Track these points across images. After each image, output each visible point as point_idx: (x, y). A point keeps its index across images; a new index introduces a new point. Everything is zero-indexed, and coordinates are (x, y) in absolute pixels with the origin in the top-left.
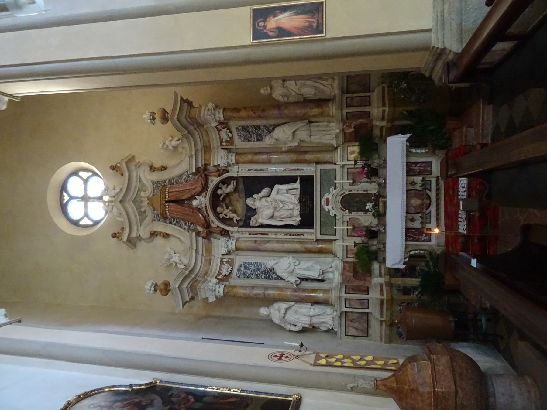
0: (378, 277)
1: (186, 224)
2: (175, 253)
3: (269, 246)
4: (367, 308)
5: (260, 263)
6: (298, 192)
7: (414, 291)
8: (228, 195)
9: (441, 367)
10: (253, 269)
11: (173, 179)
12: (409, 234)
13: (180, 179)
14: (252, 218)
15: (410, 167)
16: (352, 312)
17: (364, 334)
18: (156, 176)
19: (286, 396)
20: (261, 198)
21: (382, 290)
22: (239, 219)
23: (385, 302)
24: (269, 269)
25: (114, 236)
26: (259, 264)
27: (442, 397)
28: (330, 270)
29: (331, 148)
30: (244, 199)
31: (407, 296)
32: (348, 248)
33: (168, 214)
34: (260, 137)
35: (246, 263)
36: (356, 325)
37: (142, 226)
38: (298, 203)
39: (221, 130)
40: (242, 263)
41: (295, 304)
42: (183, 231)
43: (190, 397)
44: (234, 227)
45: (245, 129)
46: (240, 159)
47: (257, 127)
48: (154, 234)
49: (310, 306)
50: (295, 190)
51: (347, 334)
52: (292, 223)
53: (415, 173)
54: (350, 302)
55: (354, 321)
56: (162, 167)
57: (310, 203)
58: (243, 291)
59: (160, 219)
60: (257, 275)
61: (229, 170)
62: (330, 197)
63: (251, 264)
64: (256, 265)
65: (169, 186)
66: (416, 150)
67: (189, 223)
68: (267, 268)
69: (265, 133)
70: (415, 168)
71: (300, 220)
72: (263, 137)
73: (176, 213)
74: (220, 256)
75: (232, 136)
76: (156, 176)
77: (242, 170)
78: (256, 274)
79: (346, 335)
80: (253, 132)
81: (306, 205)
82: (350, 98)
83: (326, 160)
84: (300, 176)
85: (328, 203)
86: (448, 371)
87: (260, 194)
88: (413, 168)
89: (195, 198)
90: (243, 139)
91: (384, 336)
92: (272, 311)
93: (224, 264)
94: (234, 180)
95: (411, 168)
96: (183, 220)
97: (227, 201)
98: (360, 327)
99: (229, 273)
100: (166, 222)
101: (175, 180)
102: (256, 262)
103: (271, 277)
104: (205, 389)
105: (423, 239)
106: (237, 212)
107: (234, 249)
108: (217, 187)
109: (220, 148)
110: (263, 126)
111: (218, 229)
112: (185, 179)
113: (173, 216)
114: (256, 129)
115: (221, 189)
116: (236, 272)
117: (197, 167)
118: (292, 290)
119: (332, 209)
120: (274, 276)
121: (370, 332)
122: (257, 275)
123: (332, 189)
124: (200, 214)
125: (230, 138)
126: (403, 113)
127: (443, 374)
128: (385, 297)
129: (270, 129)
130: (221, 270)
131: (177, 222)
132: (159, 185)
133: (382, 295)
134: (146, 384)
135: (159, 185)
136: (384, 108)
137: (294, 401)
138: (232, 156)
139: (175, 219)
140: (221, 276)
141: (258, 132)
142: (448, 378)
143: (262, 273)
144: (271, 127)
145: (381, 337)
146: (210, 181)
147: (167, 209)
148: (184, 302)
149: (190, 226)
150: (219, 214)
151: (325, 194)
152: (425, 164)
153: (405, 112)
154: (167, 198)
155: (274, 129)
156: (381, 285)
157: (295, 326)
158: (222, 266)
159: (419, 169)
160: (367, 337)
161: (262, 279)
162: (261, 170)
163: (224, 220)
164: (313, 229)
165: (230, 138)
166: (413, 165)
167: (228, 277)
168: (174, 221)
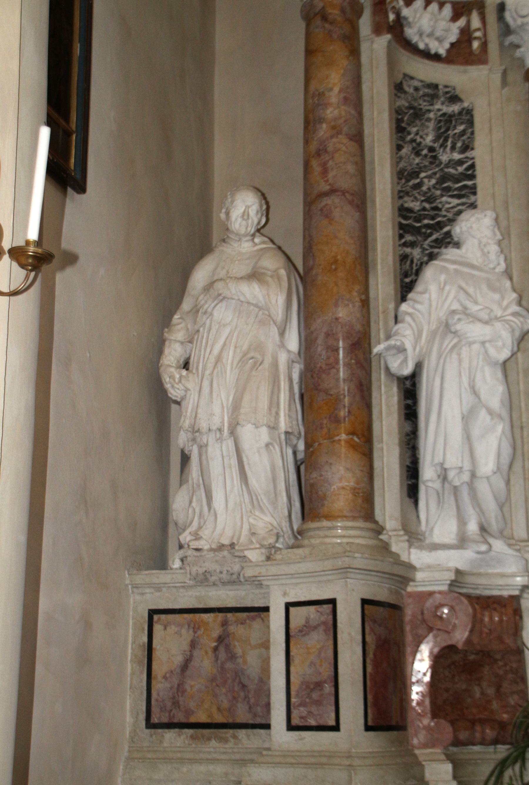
4: (295, 721)
5: (474, 187)
10: (444, 158)
16: (266, 645)
17: (163, 709)
26: (469, 183)
28: (473, 527)
35: (471, 123)
40: (466, 105)
41: (289, 352)
49: (283, 425)
51: (156, 617)
54: (315, 628)
55: (222, 654)
58: (336, 90)
60: (415, 174)
63: (466, 148)
64: (461, 169)
79: (152, 613)
93: (455, 18)
99: (415, 39)
102: (478, 167)
103: (409, 238)
116: (422, 77)
118: (358, 327)
120: (416, 253)
121: (170, 735)
122: (415, 174)
143: (429, 200)
160: (150, 725)
161: (401, 197)
168: (456, 134)
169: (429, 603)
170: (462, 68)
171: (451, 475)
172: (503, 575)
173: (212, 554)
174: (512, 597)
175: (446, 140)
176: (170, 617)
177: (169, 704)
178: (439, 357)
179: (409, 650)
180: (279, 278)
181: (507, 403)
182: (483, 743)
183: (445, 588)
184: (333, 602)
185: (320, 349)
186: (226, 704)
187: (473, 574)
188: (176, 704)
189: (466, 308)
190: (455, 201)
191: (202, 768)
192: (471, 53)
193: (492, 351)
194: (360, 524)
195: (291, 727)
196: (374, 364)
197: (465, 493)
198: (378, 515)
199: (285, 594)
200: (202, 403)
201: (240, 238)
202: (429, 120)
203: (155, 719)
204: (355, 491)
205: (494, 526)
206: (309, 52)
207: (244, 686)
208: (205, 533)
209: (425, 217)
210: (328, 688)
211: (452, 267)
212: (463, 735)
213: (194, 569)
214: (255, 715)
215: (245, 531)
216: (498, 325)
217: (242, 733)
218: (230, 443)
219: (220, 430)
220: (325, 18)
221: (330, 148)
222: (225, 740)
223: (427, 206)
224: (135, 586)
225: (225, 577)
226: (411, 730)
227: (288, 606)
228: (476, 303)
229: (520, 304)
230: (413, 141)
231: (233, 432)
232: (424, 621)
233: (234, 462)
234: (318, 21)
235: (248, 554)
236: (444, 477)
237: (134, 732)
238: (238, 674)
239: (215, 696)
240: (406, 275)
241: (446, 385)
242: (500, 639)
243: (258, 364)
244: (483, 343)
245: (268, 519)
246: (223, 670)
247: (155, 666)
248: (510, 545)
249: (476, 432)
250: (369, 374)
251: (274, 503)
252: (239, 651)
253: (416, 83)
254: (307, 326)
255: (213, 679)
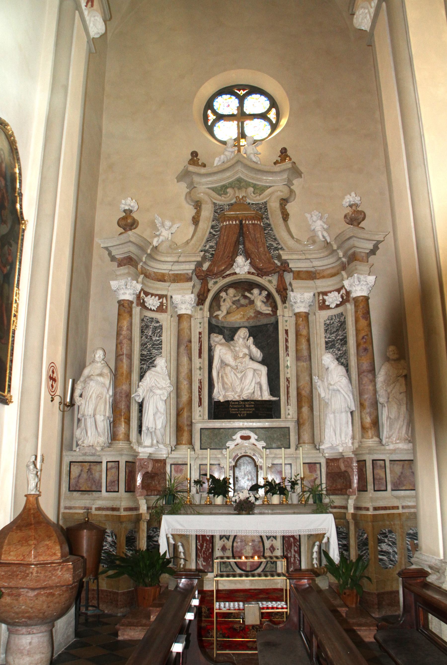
0: (147, 505)
1: (211, 247)
2: (172, 233)
3: (185, 360)
4: (108, 490)
6: (257, 397)
7: (132, 550)
8: (252, 302)
9: (60, 573)
10: (154, 339)
11: (271, 230)
12: (205, 545)
13: (272, 238)
14: (221, 337)
15: (295, 545)
16: (101, 471)
17: (73, 487)
18: (274, 205)
19: (10, 386)
20: (249, 348)
21: (131, 509)
22: (220, 318)
23: (115, 513)
24: (154, 360)
25: (194, 154)
26: (160, 346)
27: (27, 572)
28: (155, 442)
29: (317, 440)
30: (246, 324)
31: (125, 541)
32: (185, 466)
33: (225, 223)
34: (331, 346)
35: (162, 329)
36: (84, 475)
37: (207, 189)
38: (243, 398)
39: (339, 294)
40: (161, 324)
42: (203, 244)
43: (8, 267)
44: (208, 313)
45: (341, 325)
46: (301, 319)
47: (344, 341)
48: (198, 205)
50: (259, 394)
51: (72, 463)
52: (215, 391)
53: (286, 551)
54: (114, 468)
55: (89, 474)
56: (286, 215)
57: (244, 414)
58: (126, 326)
59: (217, 213)
60: (146, 344)
61: (285, 305)
62: (253, 440)
63: (160, 336)
64: (158, 342)
65: (262, 224)
66: (316, 552)
67: (213, 251)
68: (155, 357)
69: (337, 352)
70: (293, 551)
71: (220, 401)
72: (331, 350)
73: (226, 234)
74: (169, 294)
75: (331, 308)
76: (274, 205)
77: (286, 321)
78: (147, 342)
80: (337, 335)
81: (241, 409)
82: (383, 465)
83: (302, 434)
84: (280, 400)
85: (244, 438)
86: (57, 580)
87: (254, 346)
88: (293, 549)
89: (247, 260)
90: (328, 322)
91: (71, 511)
92: (99, 364)
93: (159, 299)
94: (272, 311)
95: (293, 546)
96: (216, 244)
97: (243, 301)
98: (81, 481)
100: (213, 221)
101: (270, 232)
103: (143, 362)
104: (15, 285)
105: (199, 562)
106: (229, 315)
107: (180, 312)
108: (262, 288)
109: (316, 291)
110: (345, 350)
111: (206, 290)
112: (272, 245)
113: (223, 231)
114: (341, 340)
115: (260, 294)
117: (288, 261)
119: (236, 443)
120: (145, 366)
121: (75, 493)
122: (146, 344)
123: (263, 444)
124: (225, 266)
125: (329, 306)
126: (365, 533)
127: (52, 574)
128: (123, 513)
129: (342, 359)
130: (152, 296)
131: (214, 235)
132: (263, 210)
133: (126, 509)
134: (22, 213)
135: (263, 210)
136: (371, 509)
137: (4, 396)
138: (305, 307)
139: (218, 233)
140: (144, 296)
141: (337, 343)
142: (48, 581)
144: (345, 361)
145: (70, 508)
146: (270, 278)
147: (231, 222)
148: (110, 249)
149: (209, 253)
150: (226, 291)
151: (256, 434)
152: (298, 564)
153: (365, 536)
154: (246, 222)
155: (342, 364)
156: (137, 509)
157: (81, 396)
158: (157, 297)
159: (291, 557)
160: (69, 491)
162: (287, 347)
163: (217, 298)
164: (209, 419)
165: (329, 306)
166: (296, 549)
167: (143, 305)
169: (142, 462)
170: (160, 313)
171: (150, 429)
172: (161, 454)
173: (87, 448)
174: (164, 460)
175: (155, 334)
176: (75, 463)
177: (75, 486)
178: (149, 398)
179: (137, 473)
180: (108, 376)
181: (165, 410)
182: (154, 495)
183: (147, 458)
184: (118, 462)
185: (118, 396)
186: (90, 485)
187: (154, 454)
188: (76, 485)
189: (156, 385)
190: (156, 351)
191: (84, 501)
192: (163, 309)
193: (162, 397)
194: (126, 442)
195: (107, 491)
196: (132, 399)
197: (153, 434)
198: (131, 439)
199: (106, 459)
200: (86, 408)
201: (97, 362)
202: (150, 328)
203: (71, 489)
204: (125, 434)
205: (160, 441)
206: (119, 315)
207: (94, 481)
208: (85, 442)
209: (148, 356)
210: (116, 482)
211: (153, 373)
212: (149, 493)
213: (83, 452)
214: (97, 489)
215: (96, 442)
216: (164, 391)
217: (94, 493)
218: (93, 419)
219: (91, 415)
220: (123, 306)
221: (123, 342)
222: (89, 495)
223: (148, 353)
224: (66, 455)
225: (91, 454)
226: (136, 492)
227: (107, 462)
228: (159, 384)
229: (171, 384)
230: (146, 334)
231: (94, 416)
232: (141, 466)
233: (94, 424)
234: (122, 307)
235: (97, 448)
236: (148, 429)
237: (65, 493)
238: (93, 478)
239: (87, 484)
240: (142, 373)
241: (150, 405)
242: (160, 470)
243: (101, 398)
244: (160, 395)
245: (102, 439)
246: (89, 477)
247: (71, 476)
248: (164, 446)
249: (157, 418)
250: (130, 403)
251: (104, 435)
252: (94, 473)
253: (148, 318)
254: (115, 390)
255: (87, 479)
